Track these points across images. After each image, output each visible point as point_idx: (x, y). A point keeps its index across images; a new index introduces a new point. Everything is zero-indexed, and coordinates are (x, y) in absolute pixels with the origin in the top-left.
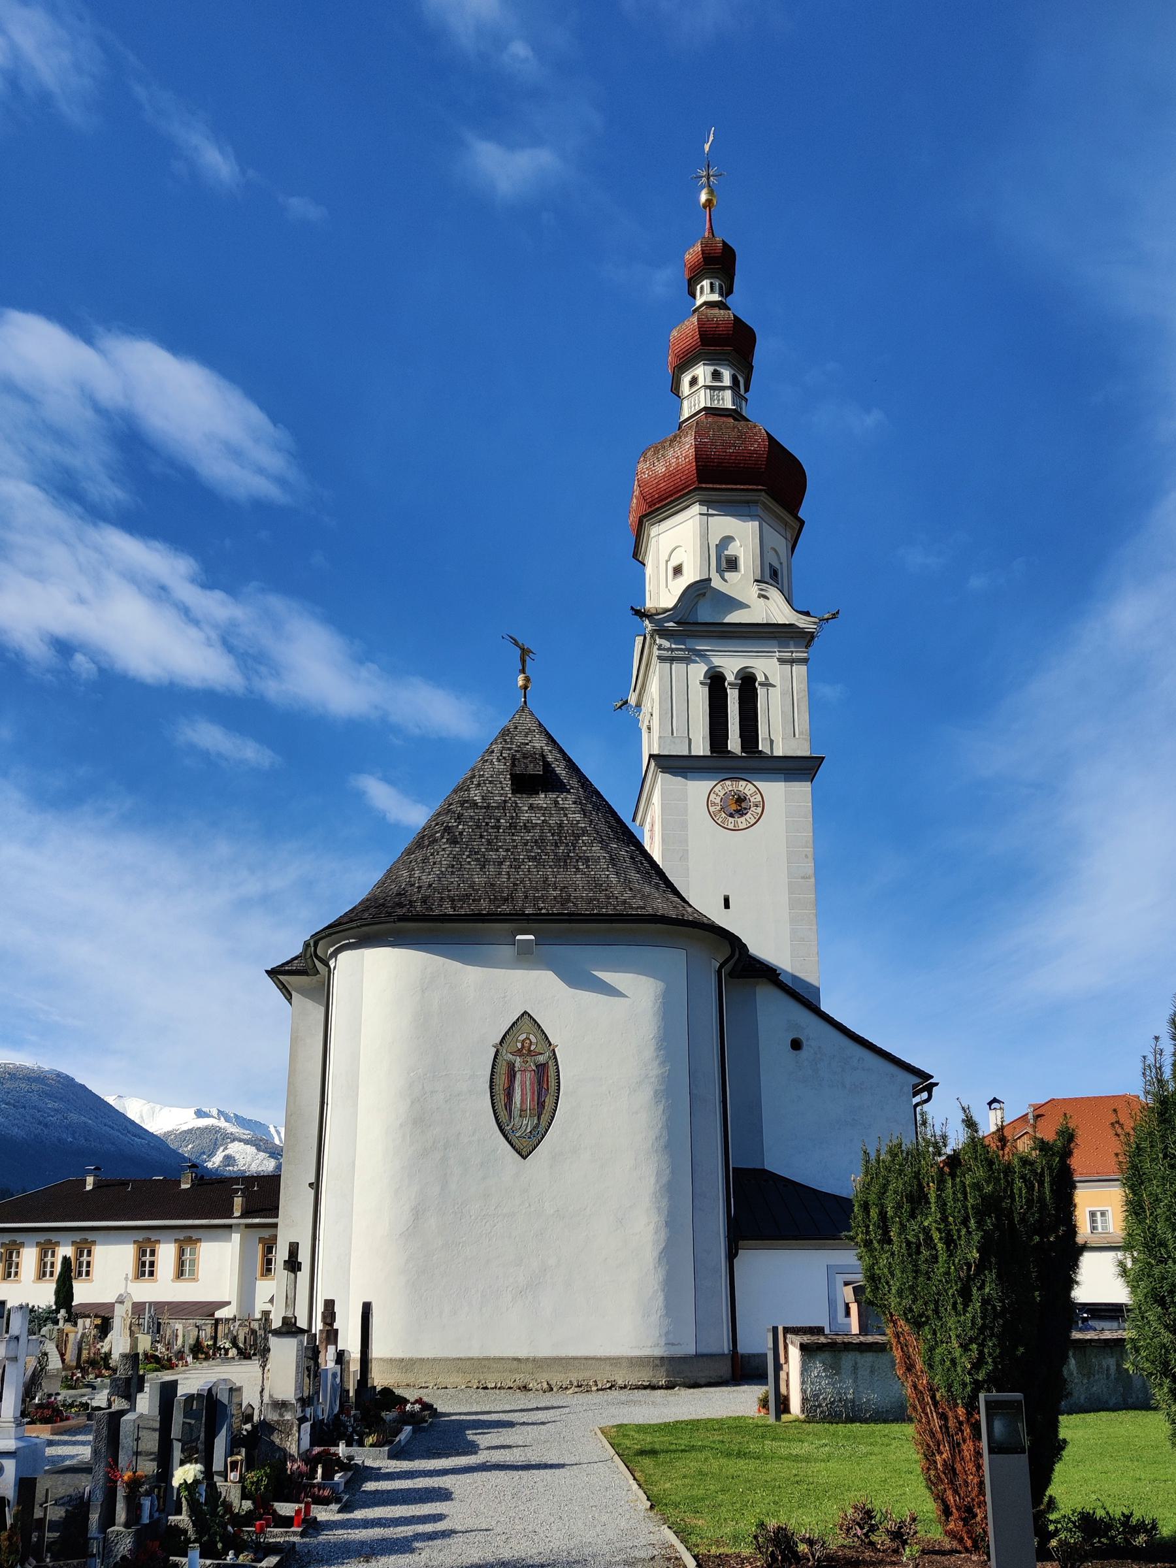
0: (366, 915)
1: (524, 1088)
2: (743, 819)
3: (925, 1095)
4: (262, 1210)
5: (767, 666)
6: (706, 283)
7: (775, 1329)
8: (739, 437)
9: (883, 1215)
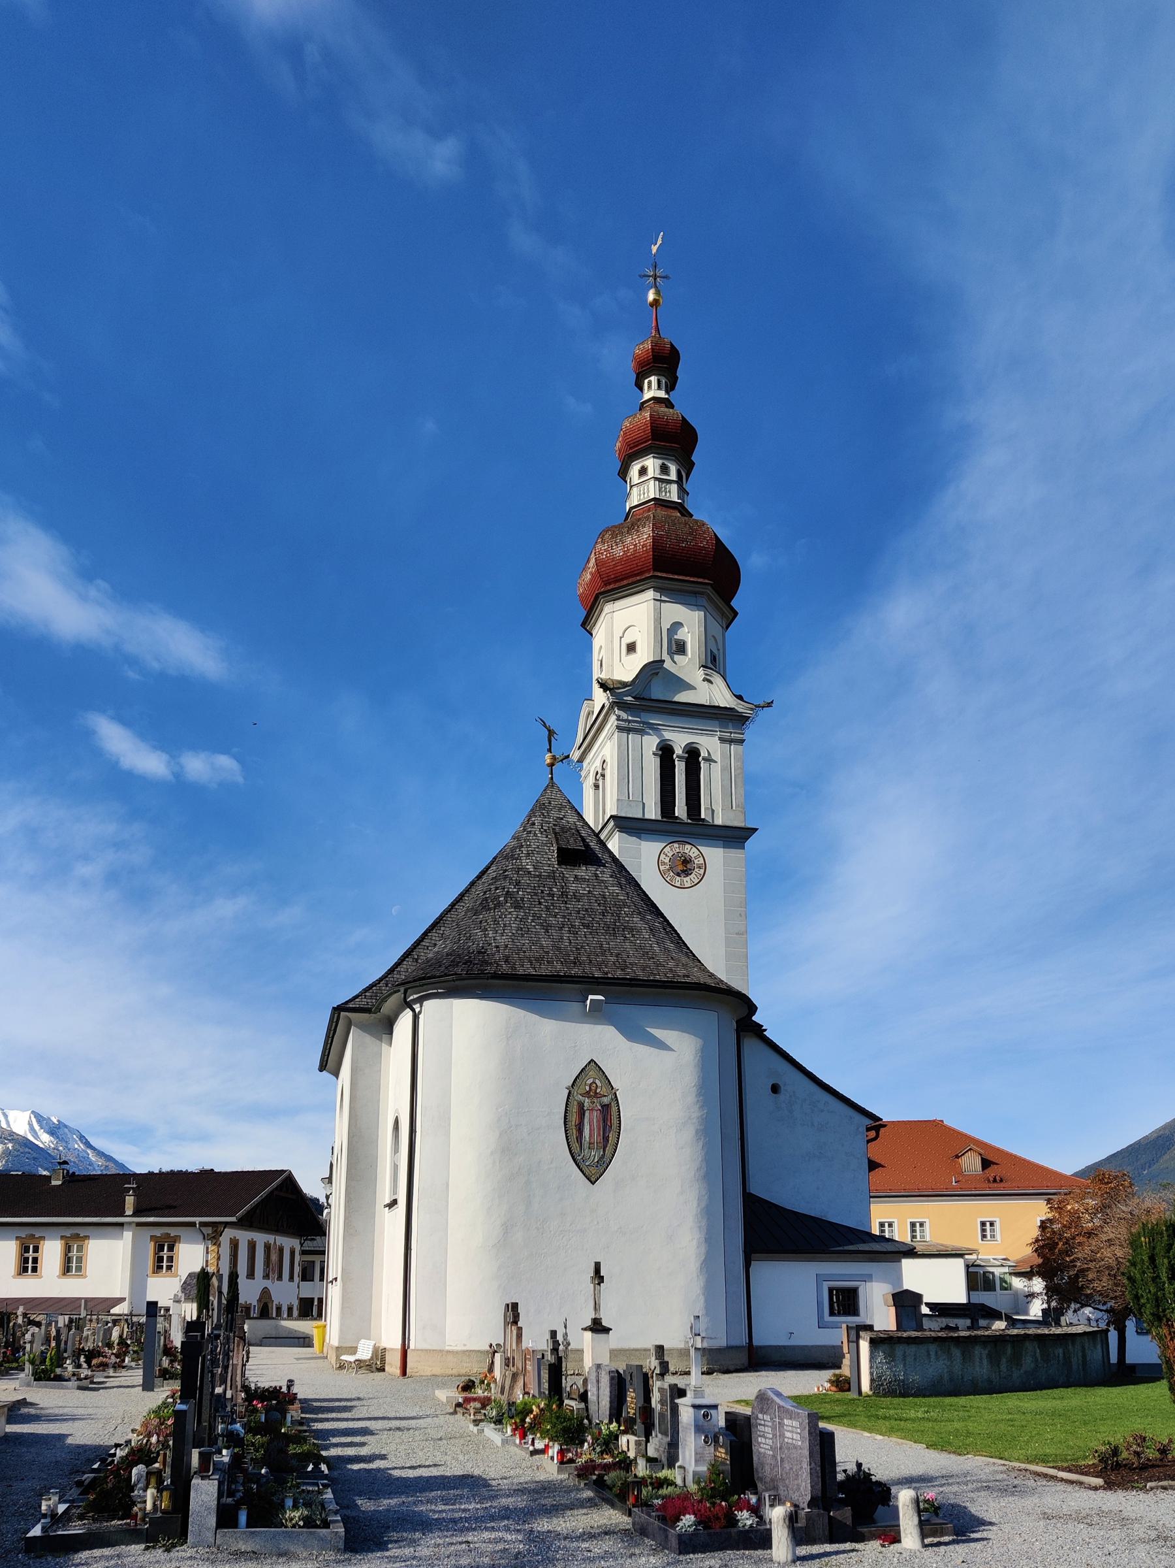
1: (592, 1124)
2: (688, 879)
4: (155, 1209)
5: (710, 744)
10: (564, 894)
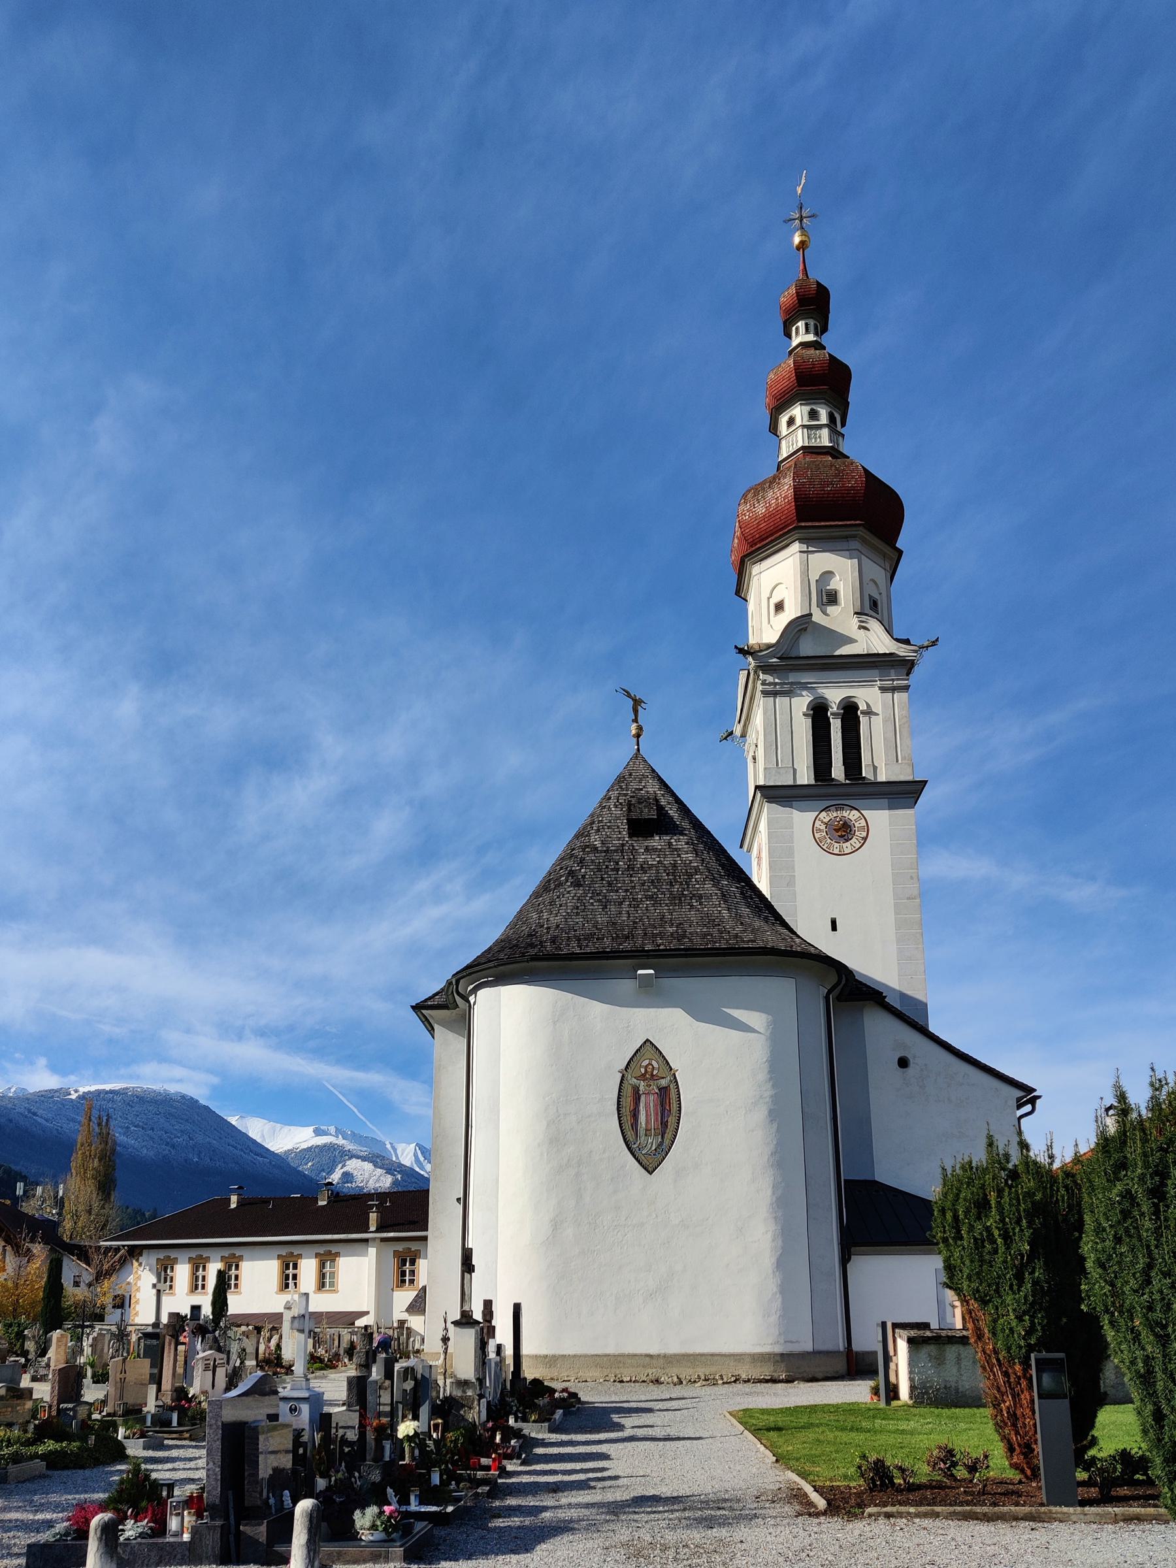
0: (502, 956)
1: (649, 1110)
2: (848, 844)
3: (1028, 1108)
5: (868, 695)
6: (801, 324)
7: (884, 1324)
8: (836, 476)
9: (956, 1217)
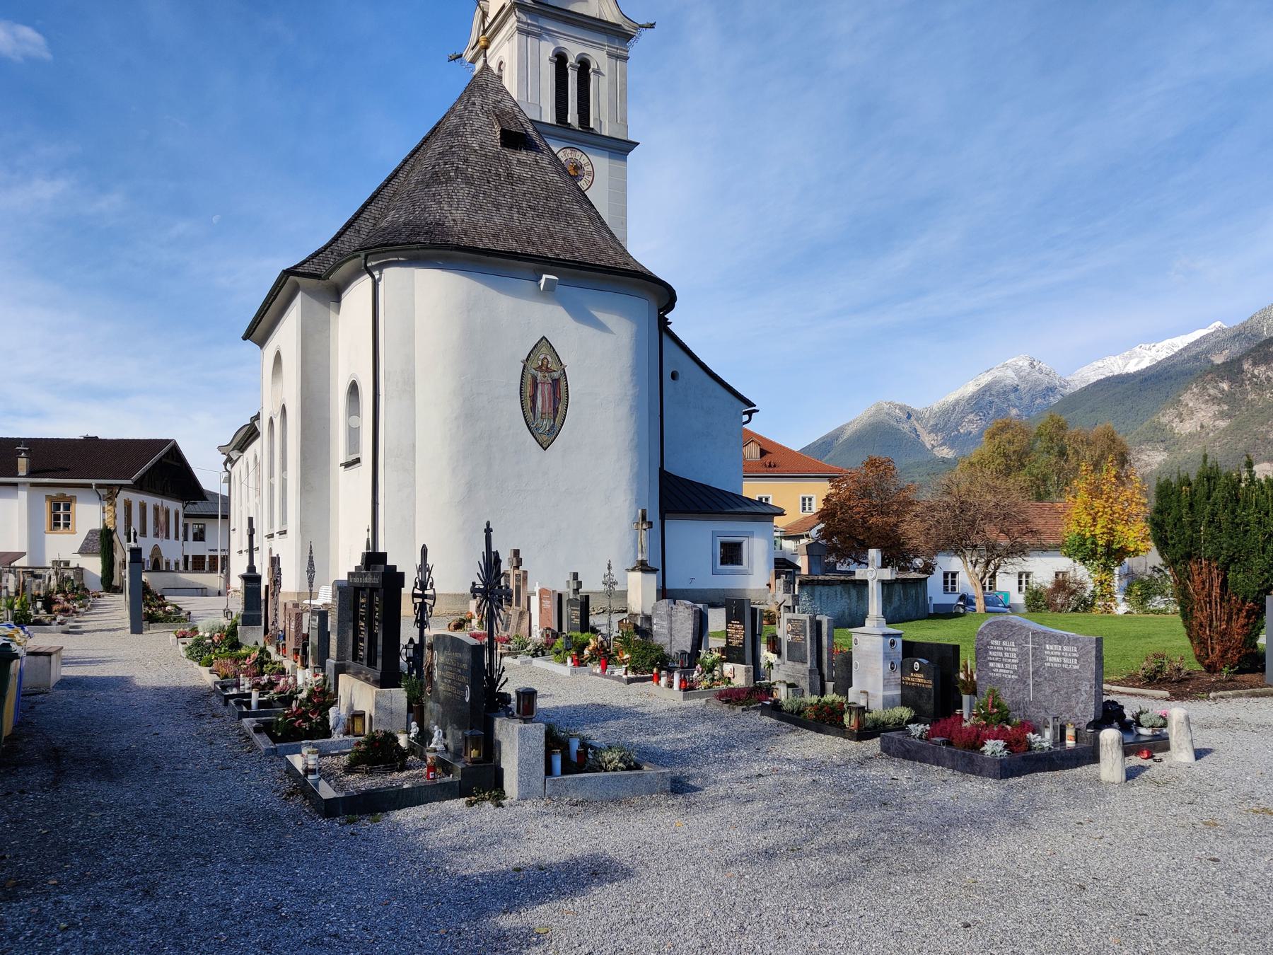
1: (544, 395)
10: (510, 175)
